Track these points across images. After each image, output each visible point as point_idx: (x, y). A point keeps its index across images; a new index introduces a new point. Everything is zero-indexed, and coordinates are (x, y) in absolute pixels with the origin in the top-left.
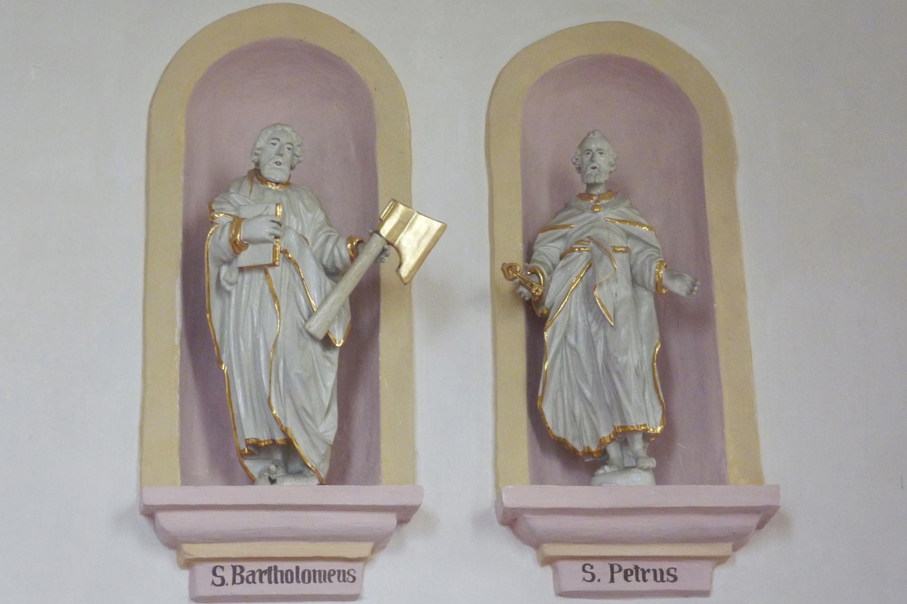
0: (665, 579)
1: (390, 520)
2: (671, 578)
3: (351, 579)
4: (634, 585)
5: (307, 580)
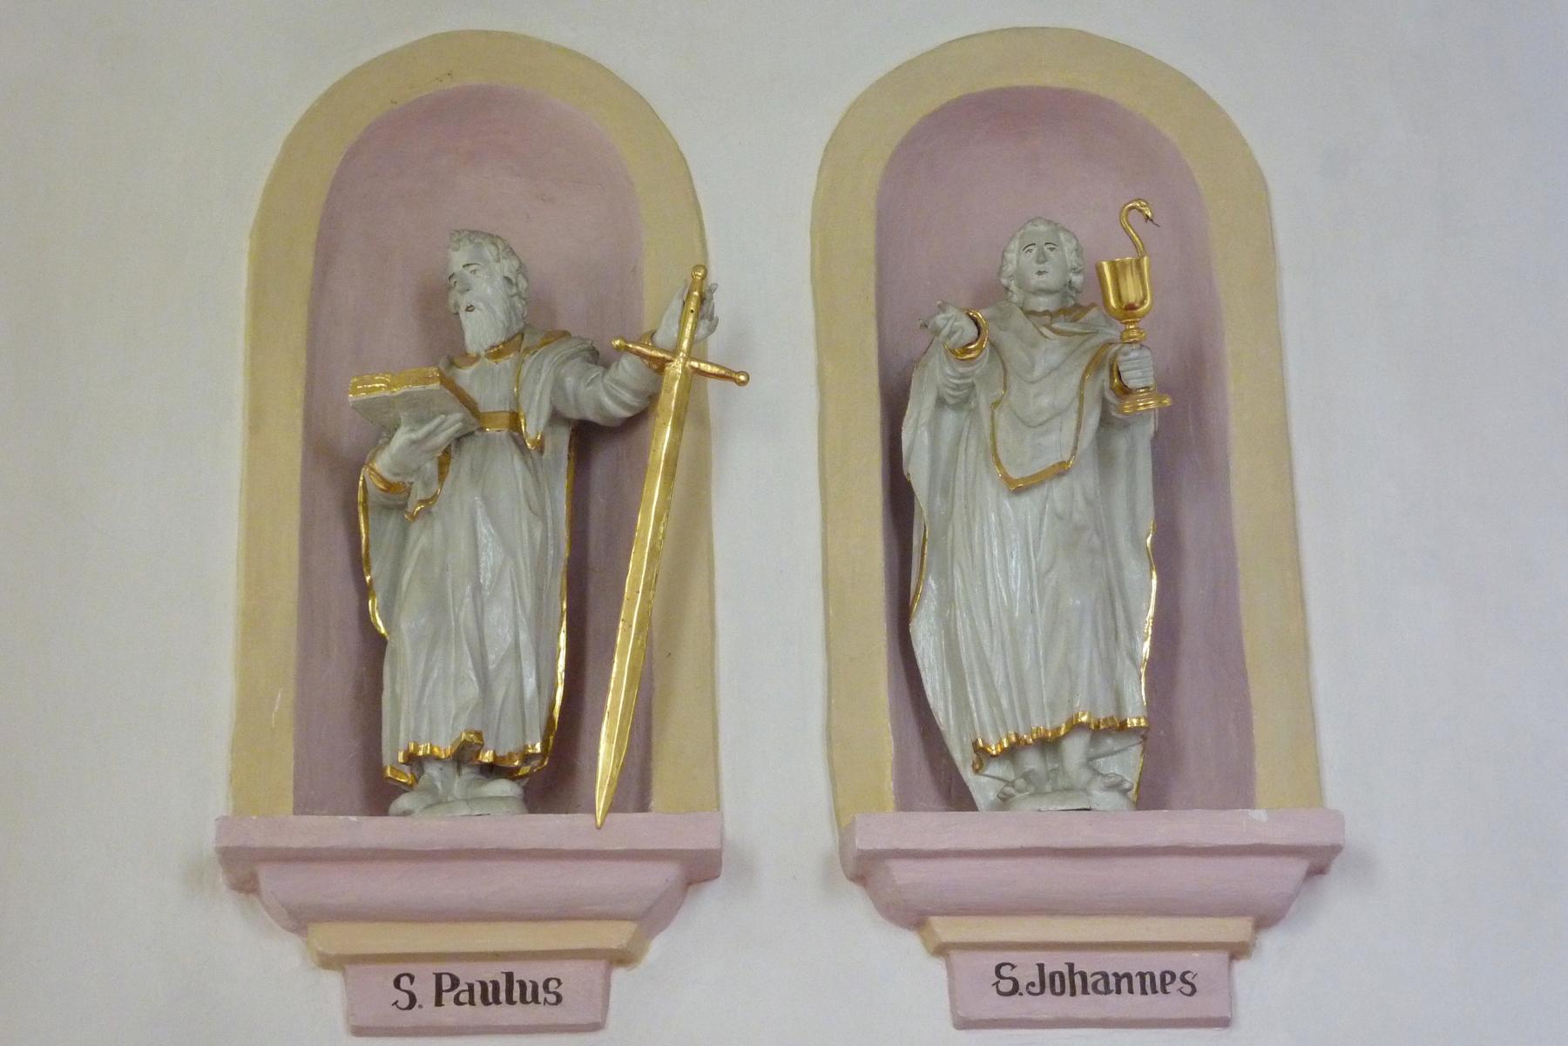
0: (541, 999)
1: (1296, 868)
2: (1188, 989)
3: (552, 998)
4: (482, 1014)
5: (1058, 990)
